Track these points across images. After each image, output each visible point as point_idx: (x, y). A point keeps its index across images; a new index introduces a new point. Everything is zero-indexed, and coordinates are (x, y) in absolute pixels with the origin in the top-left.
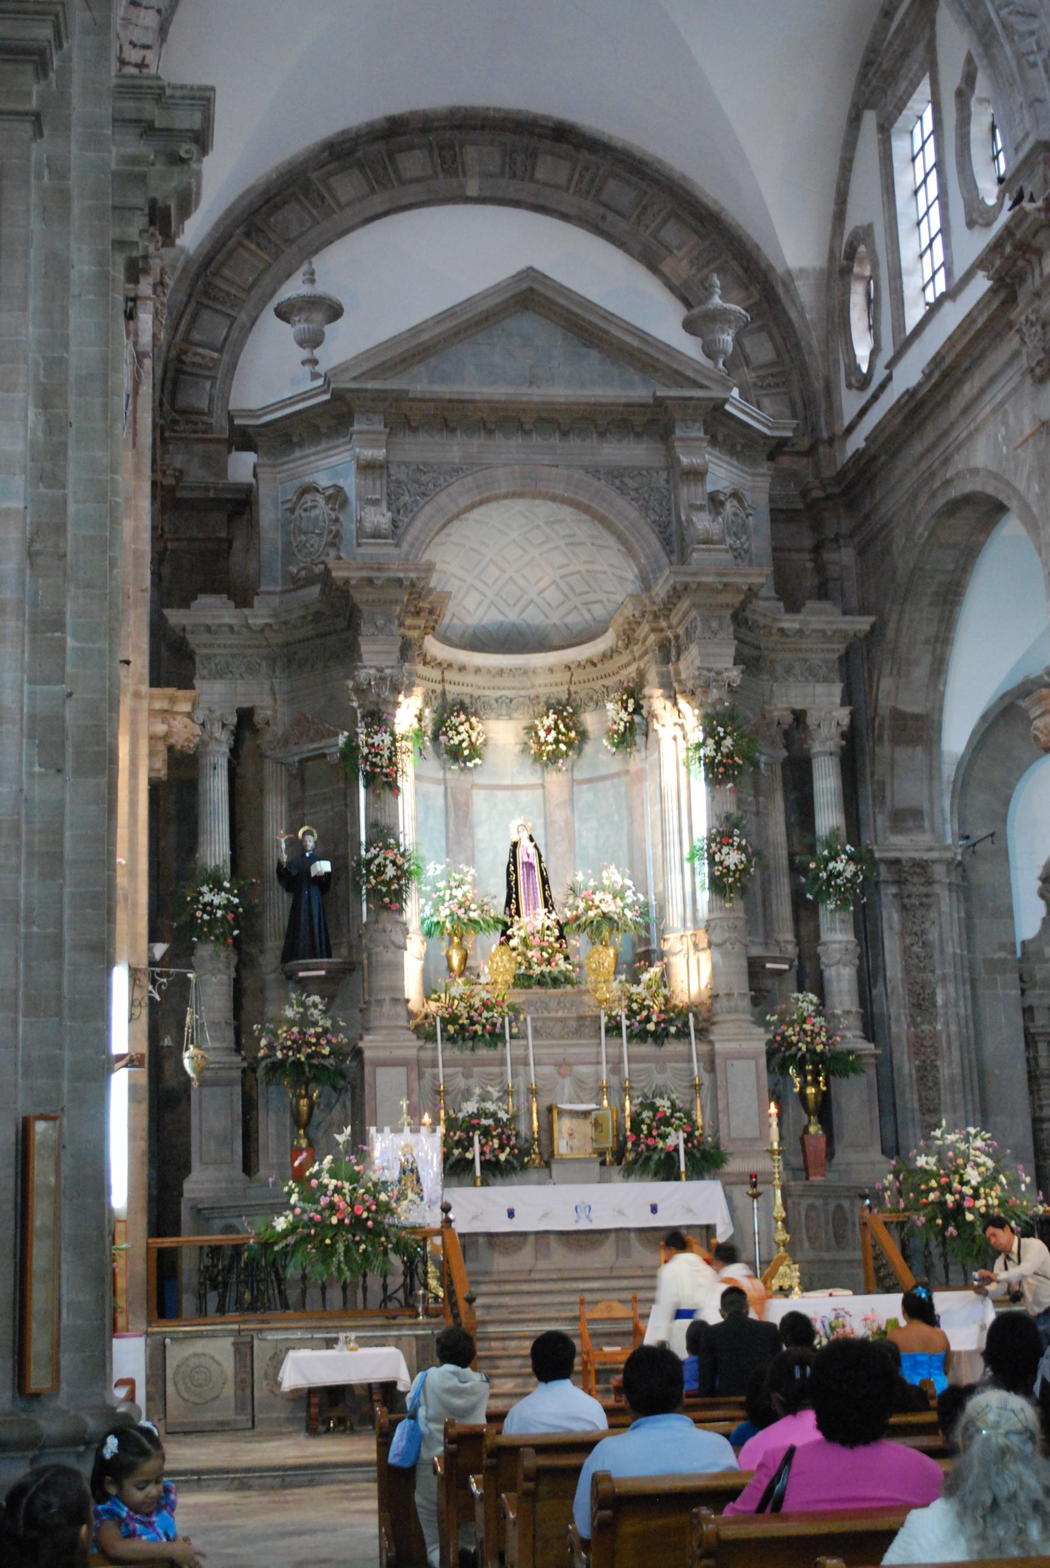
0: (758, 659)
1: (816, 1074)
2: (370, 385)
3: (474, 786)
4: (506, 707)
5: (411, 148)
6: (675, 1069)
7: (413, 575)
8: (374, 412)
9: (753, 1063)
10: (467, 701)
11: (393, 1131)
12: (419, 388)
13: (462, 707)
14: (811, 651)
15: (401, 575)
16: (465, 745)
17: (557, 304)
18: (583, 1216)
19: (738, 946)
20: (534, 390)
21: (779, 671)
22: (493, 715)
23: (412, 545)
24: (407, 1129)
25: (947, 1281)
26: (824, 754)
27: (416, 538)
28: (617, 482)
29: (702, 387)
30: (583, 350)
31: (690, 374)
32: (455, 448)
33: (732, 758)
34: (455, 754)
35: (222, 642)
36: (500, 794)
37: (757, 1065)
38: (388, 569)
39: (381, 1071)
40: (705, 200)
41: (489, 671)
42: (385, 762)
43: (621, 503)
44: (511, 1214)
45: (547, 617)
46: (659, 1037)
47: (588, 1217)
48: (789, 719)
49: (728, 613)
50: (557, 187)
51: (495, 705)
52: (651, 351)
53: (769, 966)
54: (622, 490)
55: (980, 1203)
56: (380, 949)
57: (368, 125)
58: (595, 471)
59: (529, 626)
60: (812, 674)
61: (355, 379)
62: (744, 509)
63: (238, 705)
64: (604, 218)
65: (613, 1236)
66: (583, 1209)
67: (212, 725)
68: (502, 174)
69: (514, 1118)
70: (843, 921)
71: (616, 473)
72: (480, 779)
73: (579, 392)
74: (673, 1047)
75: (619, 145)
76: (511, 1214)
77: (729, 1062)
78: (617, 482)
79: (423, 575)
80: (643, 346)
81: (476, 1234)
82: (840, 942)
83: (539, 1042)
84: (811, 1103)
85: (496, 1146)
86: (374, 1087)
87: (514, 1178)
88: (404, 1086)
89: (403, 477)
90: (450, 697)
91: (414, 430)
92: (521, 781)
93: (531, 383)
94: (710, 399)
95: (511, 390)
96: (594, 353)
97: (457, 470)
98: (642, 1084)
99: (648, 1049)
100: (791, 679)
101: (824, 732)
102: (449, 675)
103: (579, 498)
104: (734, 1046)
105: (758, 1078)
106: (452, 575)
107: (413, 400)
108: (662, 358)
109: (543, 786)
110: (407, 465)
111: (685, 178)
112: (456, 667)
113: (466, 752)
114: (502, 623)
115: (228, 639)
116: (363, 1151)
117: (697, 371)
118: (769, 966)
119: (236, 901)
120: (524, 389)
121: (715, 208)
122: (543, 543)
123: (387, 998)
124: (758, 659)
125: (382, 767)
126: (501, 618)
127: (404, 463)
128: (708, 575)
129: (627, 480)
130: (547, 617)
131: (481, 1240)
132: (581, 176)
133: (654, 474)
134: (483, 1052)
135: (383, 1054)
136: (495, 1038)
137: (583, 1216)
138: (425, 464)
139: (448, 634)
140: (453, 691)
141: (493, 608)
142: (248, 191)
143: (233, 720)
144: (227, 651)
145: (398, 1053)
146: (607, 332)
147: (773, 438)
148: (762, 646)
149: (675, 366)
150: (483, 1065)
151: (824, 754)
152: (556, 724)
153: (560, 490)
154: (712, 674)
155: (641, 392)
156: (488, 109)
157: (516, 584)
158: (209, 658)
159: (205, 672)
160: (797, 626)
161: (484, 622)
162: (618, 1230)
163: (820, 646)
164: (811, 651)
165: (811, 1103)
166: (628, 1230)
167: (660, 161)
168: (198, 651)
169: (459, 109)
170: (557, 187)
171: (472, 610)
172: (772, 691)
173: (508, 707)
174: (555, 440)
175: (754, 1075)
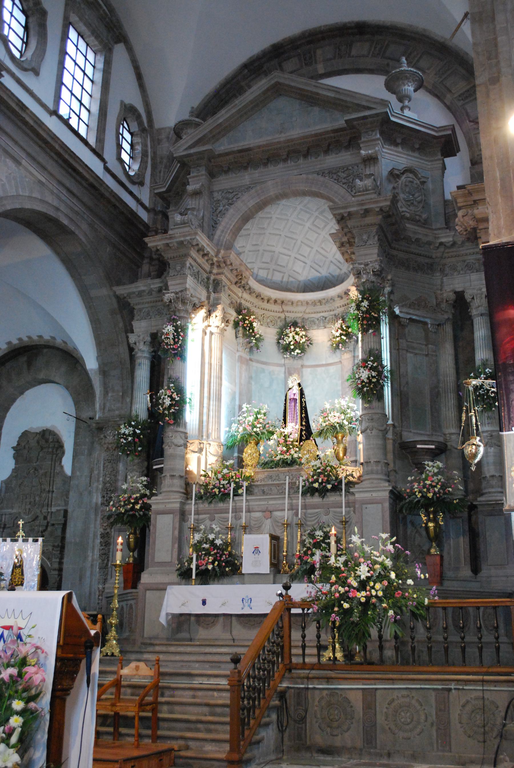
0: (432, 265)
1: (435, 513)
2: (192, 151)
3: (302, 366)
4: (324, 322)
5: (289, 58)
6: (335, 512)
7: (188, 238)
8: (200, 166)
9: (380, 506)
10: (299, 321)
11: (12, 541)
12: (222, 148)
13: (295, 324)
14: (466, 255)
15: (182, 239)
16: (292, 343)
17: (292, 87)
18: (246, 604)
19: (374, 432)
20: (283, 135)
21: (447, 270)
22: (316, 327)
23: (222, 231)
24: (20, 539)
25: (464, 661)
26: (478, 315)
27: (225, 227)
28: (335, 177)
29: (369, 108)
30: (310, 108)
31: (364, 103)
32: (247, 177)
33: (370, 314)
34: (286, 349)
35: (145, 301)
36: (319, 369)
37: (383, 507)
38: (175, 237)
39: (159, 517)
40: (436, 38)
41: (307, 303)
42: (172, 342)
43: (336, 187)
44: (204, 602)
45: (341, 269)
46: (322, 492)
47: (249, 606)
48: (452, 296)
49: (374, 229)
50: (363, 56)
51: (317, 322)
52: (342, 97)
53: (418, 446)
54: (338, 180)
55: (362, 595)
56: (167, 447)
57: (262, 51)
58: (322, 173)
59: (333, 276)
60: (470, 268)
61: (186, 149)
62: (419, 179)
63: (150, 332)
64: (388, 65)
65: (221, 619)
66: (247, 601)
67: (139, 342)
68: (334, 58)
69: (226, 544)
70: (489, 418)
71: (334, 171)
72: (306, 363)
73: (306, 130)
74: (332, 498)
75: (389, 24)
76: (204, 602)
77: (364, 506)
78: (335, 177)
79: (193, 237)
80: (338, 96)
81: (190, 615)
82: (487, 431)
83: (249, 498)
84: (432, 534)
85: (210, 561)
86: (155, 527)
87: (225, 580)
88: (171, 526)
89: (220, 198)
90: (288, 320)
91: (226, 172)
92: (331, 361)
93: (281, 132)
94: (377, 115)
95: (269, 138)
96: (316, 109)
97: (248, 188)
98: (313, 523)
99: (316, 499)
100: (455, 274)
101: (476, 302)
102: (286, 308)
103: (314, 189)
104: (367, 495)
105: (383, 516)
106: (280, 253)
107: (220, 155)
108: (348, 99)
109: (340, 362)
110: (222, 191)
111: (425, 30)
112: (279, 302)
113: (292, 347)
114: (320, 278)
115: (148, 299)
116: (304, 577)
117: (367, 101)
118: (418, 446)
119: (138, 431)
120: (277, 136)
121: (442, 40)
122: (325, 226)
123: (168, 475)
124: (432, 265)
125: (170, 345)
126: (318, 275)
127: (220, 190)
128: (353, 206)
129: (339, 174)
130: (341, 269)
131: (193, 619)
132: (375, 48)
133: (356, 167)
134: (221, 505)
135: (161, 507)
136: (225, 496)
137: (246, 604)
138: (231, 188)
139: (289, 287)
140: (291, 316)
141: (313, 270)
142: (207, 95)
143: (149, 339)
144: (147, 305)
145: (170, 506)
146: (318, 94)
147: (442, 137)
148: (434, 256)
149: (356, 102)
150: (221, 513)
151: (478, 315)
152: (341, 326)
153: (302, 187)
154: (363, 266)
155: (340, 122)
156: (321, 27)
157: (321, 254)
158: (140, 310)
159: (139, 317)
160: (451, 239)
161: (309, 278)
162: (224, 615)
163: (472, 251)
164: (466, 255)
165: (432, 534)
166: (231, 615)
167: (411, 26)
168: (136, 307)
169: (306, 31)
170: (363, 56)
171: (300, 272)
172: (442, 283)
173: (324, 322)
174: (301, 161)
175: (380, 514)
